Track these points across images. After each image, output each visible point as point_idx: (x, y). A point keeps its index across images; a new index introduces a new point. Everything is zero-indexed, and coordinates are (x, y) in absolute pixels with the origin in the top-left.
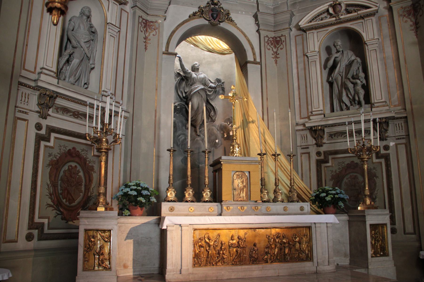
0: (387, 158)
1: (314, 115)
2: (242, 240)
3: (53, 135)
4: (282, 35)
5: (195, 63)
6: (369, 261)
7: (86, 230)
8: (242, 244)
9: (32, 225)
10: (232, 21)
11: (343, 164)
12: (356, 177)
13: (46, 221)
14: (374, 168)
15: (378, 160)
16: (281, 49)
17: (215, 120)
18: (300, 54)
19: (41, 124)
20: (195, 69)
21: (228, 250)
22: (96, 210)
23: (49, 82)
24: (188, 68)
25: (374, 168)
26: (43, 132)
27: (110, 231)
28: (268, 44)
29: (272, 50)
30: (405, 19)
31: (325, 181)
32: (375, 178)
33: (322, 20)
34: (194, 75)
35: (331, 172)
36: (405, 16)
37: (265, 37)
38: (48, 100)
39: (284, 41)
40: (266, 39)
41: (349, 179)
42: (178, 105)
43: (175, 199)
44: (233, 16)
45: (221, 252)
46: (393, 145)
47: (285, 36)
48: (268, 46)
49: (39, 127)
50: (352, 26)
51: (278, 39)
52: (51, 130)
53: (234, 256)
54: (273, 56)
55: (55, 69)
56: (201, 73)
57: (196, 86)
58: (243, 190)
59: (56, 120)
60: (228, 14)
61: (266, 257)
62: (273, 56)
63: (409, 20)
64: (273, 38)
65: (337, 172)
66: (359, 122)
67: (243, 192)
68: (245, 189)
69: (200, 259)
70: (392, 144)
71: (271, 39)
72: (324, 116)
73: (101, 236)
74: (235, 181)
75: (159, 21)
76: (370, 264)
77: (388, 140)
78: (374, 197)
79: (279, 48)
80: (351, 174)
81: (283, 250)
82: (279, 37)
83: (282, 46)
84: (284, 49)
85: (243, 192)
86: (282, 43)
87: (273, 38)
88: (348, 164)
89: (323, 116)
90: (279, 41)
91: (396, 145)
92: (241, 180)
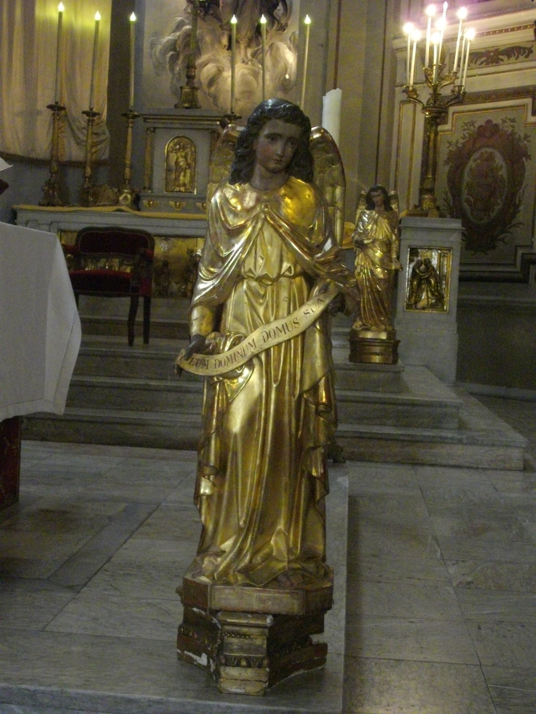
6: (400, 315)
11: (472, 128)
12: (491, 158)
14: (526, 137)
17: (286, 25)
25: (526, 137)
32: (524, 159)
35: (448, 145)
43: (157, 241)
58: (185, 173)
65: (460, 145)
67: (184, 176)
68: (188, 171)
74: (171, 155)
78: (517, 202)
80: (483, 150)
88: (481, 126)
92: (183, 154)
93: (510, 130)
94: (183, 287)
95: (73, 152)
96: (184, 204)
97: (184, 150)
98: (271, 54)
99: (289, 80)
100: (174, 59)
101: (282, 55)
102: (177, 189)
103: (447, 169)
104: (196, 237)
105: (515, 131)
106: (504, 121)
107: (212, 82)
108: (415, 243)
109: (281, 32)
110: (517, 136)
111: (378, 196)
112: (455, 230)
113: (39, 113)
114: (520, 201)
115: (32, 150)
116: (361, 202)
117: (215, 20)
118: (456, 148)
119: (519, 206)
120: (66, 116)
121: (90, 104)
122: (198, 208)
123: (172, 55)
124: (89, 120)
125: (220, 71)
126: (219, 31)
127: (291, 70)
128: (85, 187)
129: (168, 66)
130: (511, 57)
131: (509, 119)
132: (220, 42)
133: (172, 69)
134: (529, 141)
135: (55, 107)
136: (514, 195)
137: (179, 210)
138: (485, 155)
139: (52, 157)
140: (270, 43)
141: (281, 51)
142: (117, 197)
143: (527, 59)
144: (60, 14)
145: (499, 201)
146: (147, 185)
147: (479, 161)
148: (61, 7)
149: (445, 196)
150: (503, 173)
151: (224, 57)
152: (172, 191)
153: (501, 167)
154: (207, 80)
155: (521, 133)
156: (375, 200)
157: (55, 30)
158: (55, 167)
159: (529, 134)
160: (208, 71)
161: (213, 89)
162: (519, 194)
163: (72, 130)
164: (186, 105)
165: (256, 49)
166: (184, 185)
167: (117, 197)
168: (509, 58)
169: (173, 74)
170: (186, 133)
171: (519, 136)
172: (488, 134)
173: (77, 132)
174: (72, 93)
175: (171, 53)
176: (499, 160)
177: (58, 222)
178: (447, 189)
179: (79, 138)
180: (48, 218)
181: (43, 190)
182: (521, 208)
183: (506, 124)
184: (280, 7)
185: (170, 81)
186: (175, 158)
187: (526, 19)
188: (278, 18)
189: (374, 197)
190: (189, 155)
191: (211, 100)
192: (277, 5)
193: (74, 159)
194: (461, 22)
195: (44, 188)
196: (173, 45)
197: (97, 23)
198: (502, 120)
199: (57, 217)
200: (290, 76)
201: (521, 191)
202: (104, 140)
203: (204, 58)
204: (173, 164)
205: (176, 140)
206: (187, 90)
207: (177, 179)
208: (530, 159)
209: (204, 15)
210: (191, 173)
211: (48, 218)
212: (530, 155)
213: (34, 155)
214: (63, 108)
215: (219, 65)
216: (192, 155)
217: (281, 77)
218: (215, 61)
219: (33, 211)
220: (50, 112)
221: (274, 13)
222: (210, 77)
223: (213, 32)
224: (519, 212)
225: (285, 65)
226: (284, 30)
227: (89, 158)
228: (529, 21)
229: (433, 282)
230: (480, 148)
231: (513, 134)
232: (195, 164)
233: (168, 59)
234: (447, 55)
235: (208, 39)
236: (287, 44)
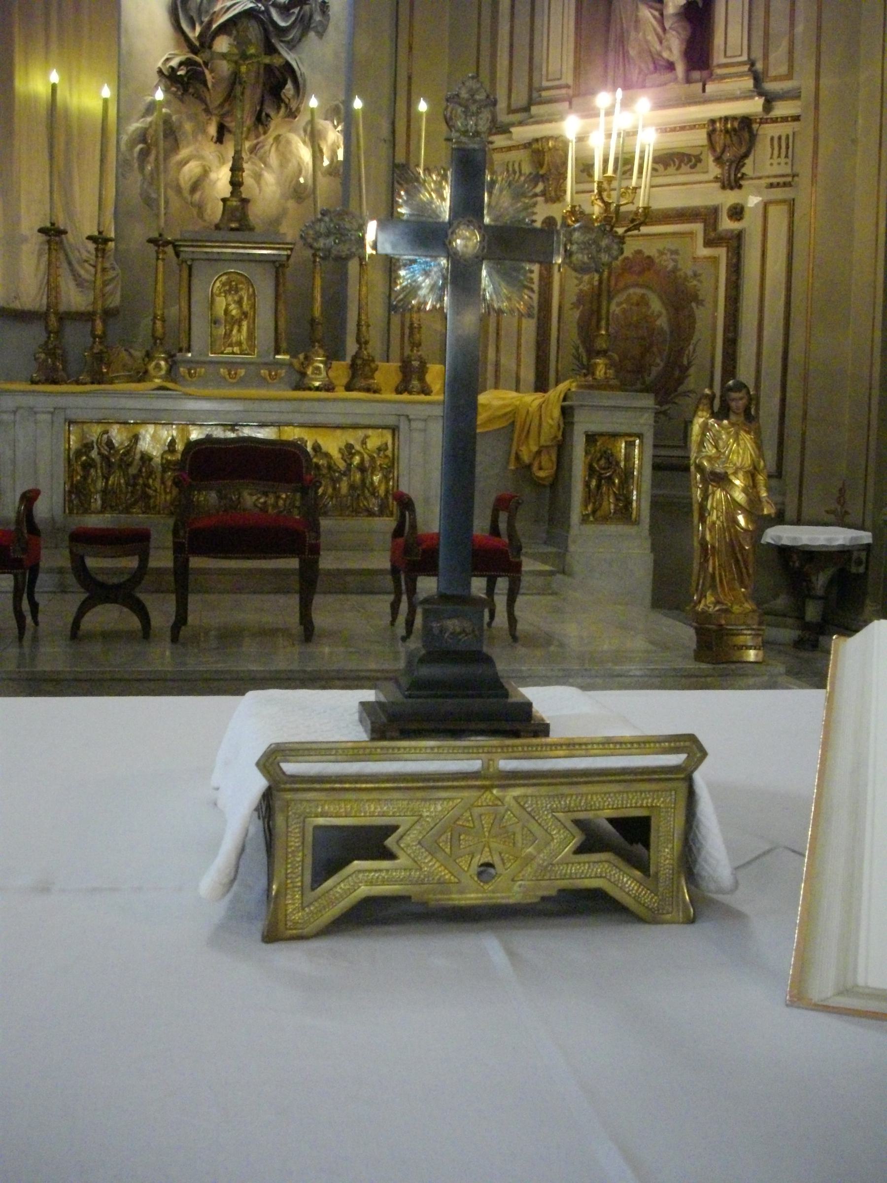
1: (775, 120)
7: (591, 438)
12: (643, 302)
14: (695, 275)
21: (159, 475)
25: (695, 275)
31: (560, 308)
32: (694, 305)
41: (624, 306)
42: (181, 64)
45: (141, 481)
46: (756, 205)
58: (240, 326)
67: (239, 331)
68: (245, 323)
69: (85, 495)
70: (753, 201)
74: (218, 299)
76: (574, 542)
77: (744, 189)
78: (685, 362)
80: (631, 291)
85: (239, 331)
91: (766, 205)
92: (236, 298)
93: (671, 265)
94: (262, 500)
95: (75, 298)
96: (242, 372)
97: (237, 291)
98: (277, 149)
99: (305, 186)
100: (144, 154)
101: (295, 151)
103: (577, 314)
105: (680, 266)
106: (661, 253)
108: (594, 428)
109: (290, 119)
110: (681, 273)
111: (741, 399)
112: (643, 409)
113: (25, 240)
114: (689, 363)
115: (15, 298)
116: (701, 407)
117: (198, 101)
118: (588, 286)
119: (687, 368)
120: (61, 242)
121: (99, 224)
122: (265, 379)
123: (141, 150)
124: (97, 249)
125: (206, 172)
126: (203, 117)
127: (307, 171)
128: (51, 346)
129: (136, 165)
130: (670, 165)
131: (669, 250)
132: (204, 131)
133: (142, 168)
134: (699, 281)
135: (51, 230)
136: (681, 352)
137: (235, 381)
138: (635, 299)
139: (48, 306)
140: (276, 133)
141: (294, 146)
142: (145, 365)
143: (693, 170)
144: (54, 87)
145: (658, 360)
146: (184, 345)
147: (624, 306)
148: (54, 77)
149: (574, 351)
150: (662, 322)
151: (210, 150)
152: (222, 353)
153: (659, 315)
154: (190, 183)
155: (686, 268)
156: (733, 404)
157: (43, 111)
158: (53, 319)
159: (699, 272)
160: (190, 171)
161: (197, 196)
162: (687, 352)
163: (70, 263)
164: (233, 225)
165: (255, 142)
166: (239, 344)
167: (145, 365)
168: (666, 169)
169: (144, 175)
171: (686, 274)
172: (637, 269)
173: (77, 267)
174: (70, 214)
175: (141, 146)
176: (656, 305)
177: (65, 409)
178: (579, 342)
179: (80, 276)
180: (50, 403)
181: (36, 359)
182: (692, 371)
183: (664, 257)
184: (289, 85)
185: (139, 184)
186: (224, 304)
187: (700, 116)
188: (287, 101)
189: (733, 400)
190: (245, 299)
191: (195, 211)
192: (285, 83)
193: (74, 309)
194: (602, 113)
195: (37, 356)
196: (143, 136)
197: (106, 101)
198: (659, 251)
199: (61, 401)
200: (305, 179)
201: (691, 347)
202: (113, 278)
203: (184, 153)
205: (224, 278)
206: (235, 203)
207: (228, 335)
208: (703, 305)
209: (183, 94)
210: (248, 327)
211: (50, 403)
212: (703, 301)
213: (17, 305)
214: (61, 232)
215: (204, 163)
216: (248, 299)
217: (291, 182)
218: (200, 158)
219: (24, 393)
220: (43, 238)
221: (283, 96)
222: (193, 180)
223: (192, 117)
224: (687, 376)
225: (299, 164)
226: (296, 117)
227: (100, 306)
228: (701, 120)
229: (617, 481)
230: (626, 287)
231: (675, 270)
232: (255, 313)
233: (135, 155)
234: (625, 163)
235: (188, 126)
236: (299, 135)
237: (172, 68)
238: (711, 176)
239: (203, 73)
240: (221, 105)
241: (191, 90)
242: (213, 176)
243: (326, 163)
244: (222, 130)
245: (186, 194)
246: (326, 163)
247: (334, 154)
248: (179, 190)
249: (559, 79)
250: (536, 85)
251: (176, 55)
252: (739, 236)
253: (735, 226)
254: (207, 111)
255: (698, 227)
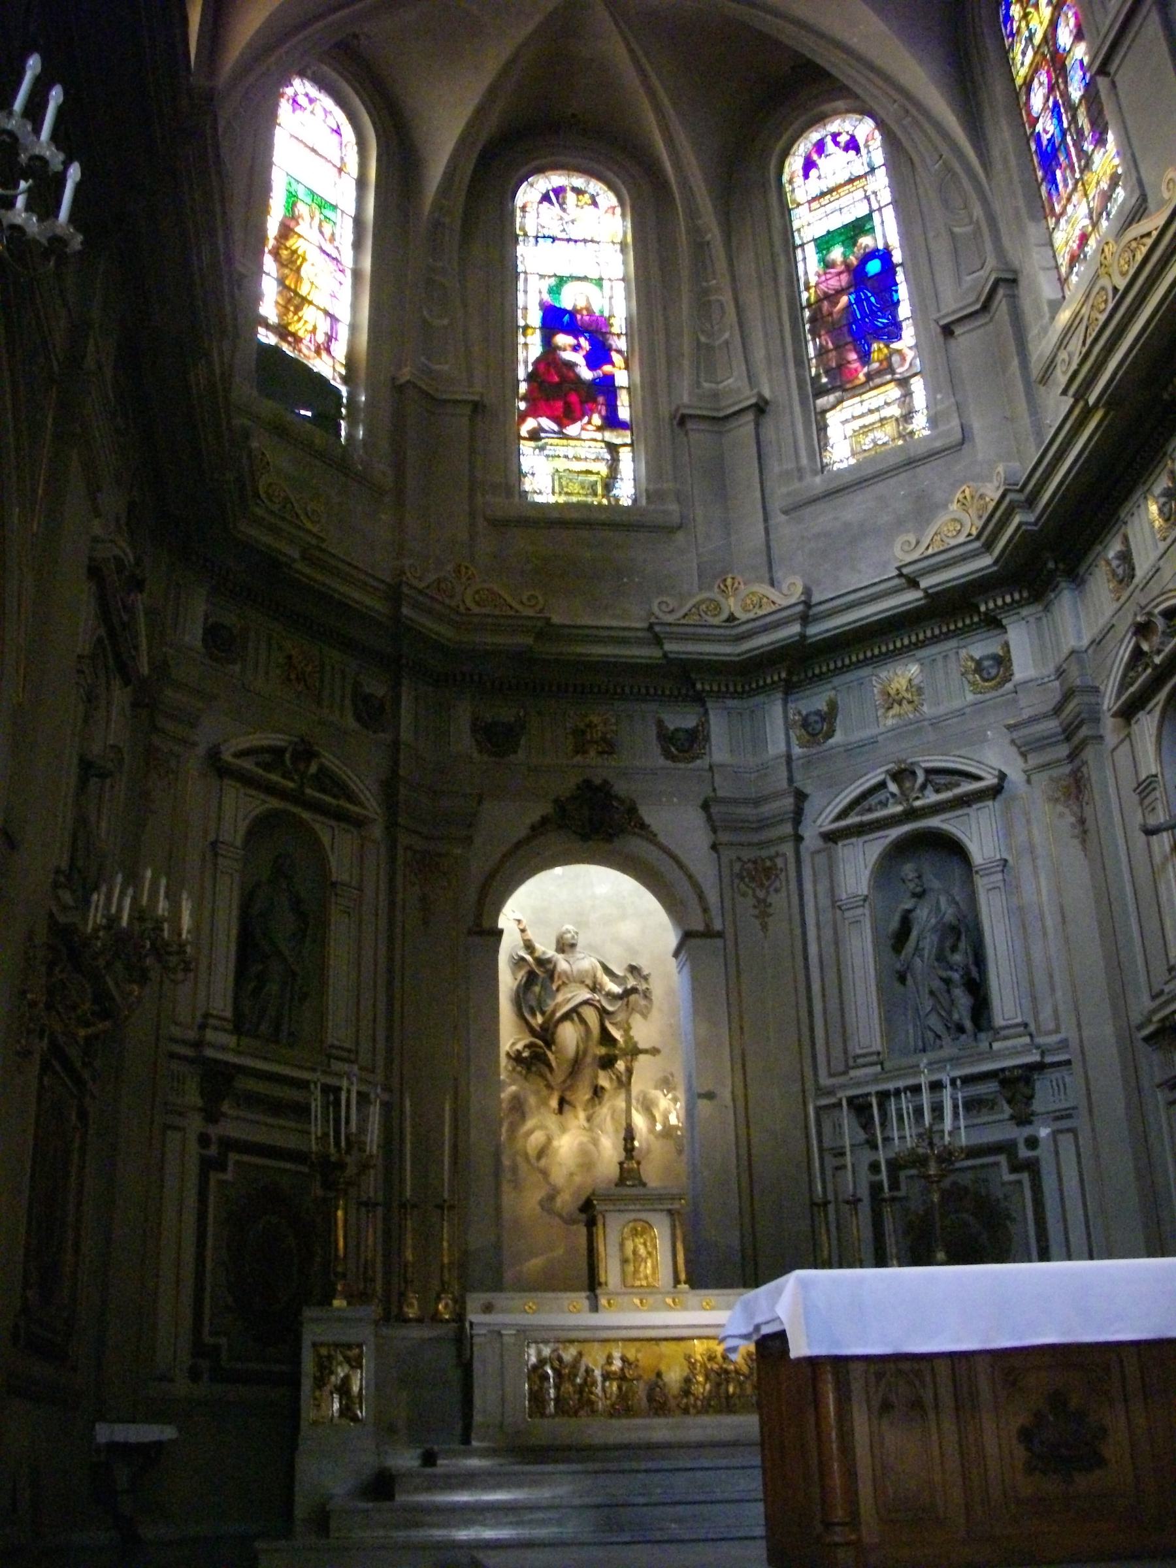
0: (1032, 1167)
2: (630, 1364)
3: (233, 1157)
4: (777, 855)
5: (564, 929)
8: (629, 1373)
9: (199, 1349)
10: (643, 826)
13: (223, 1341)
15: (1013, 1177)
16: (777, 891)
18: (825, 902)
19: (207, 1135)
20: (565, 946)
22: (330, 1304)
23: (222, 1045)
24: (545, 948)
25: (1006, 1197)
26: (213, 1151)
27: (360, 1346)
28: (742, 879)
29: (755, 896)
30: (1060, 808)
33: (870, 810)
34: (562, 964)
36: (1057, 800)
37: (731, 861)
38: (218, 1081)
39: (781, 870)
40: (737, 867)
42: (525, 1046)
44: (651, 815)
46: (1048, 1135)
47: (784, 855)
48: (742, 886)
49: (204, 1140)
50: (945, 826)
51: (768, 863)
52: (228, 1144)
53: (614, 1399)
54: (756, 912)
55: (228, 1014)
56: (582, 955)
57: (569, 996)
59: (237, 1125)
60: (632, 810)
61: (685, 1400)
62: (756, 912)
63: (1067, 811)
64: (755, 862)
66: (916, 1089)
70: (1044, 1132)
71: (750, 866)
72: (883, 1069)
73: (345, 1357)
75: (455, 851)
79: (771, 889)
81: (723, 1387)
82: (771, 859)
83: (777, 884)
84: (783, 894)
86: (777, 876)
87: (755, 862)
89: (879, 1067)
90: (770, 868)
91: (1055, 1133)
102: (638, 1283)
104: (692, 1338)
107: (543, 1152)
125: (549, 1140)
126: (545, 1092)
151: (551, 1121)
152: (633, 1286)
161: (543, 1162)
170: (643, 1215)
203: (530, 1124)
204: (631, 1256)
207: (636, 1271)
223: (537, 1093)
235: (532, 1100)
237: (518, 1051)
238: (1006, 1116)
239: (546, 1055)
240: (564, 1082)
241: (534, 1069)
242: (555, 1143)
243: (659, 1127)
244: (562, 1102)
245: (533, 1161)
246: (659, 1127)
247: (666, 1118)
248: (526, 1156)
249: (1061, 1131)
250: (851, 1053)
251: (520, 1040)
252: (1036, 1161)
253: (1030, 1154)
254: (549, 1087)
255: (1002, 1159)
